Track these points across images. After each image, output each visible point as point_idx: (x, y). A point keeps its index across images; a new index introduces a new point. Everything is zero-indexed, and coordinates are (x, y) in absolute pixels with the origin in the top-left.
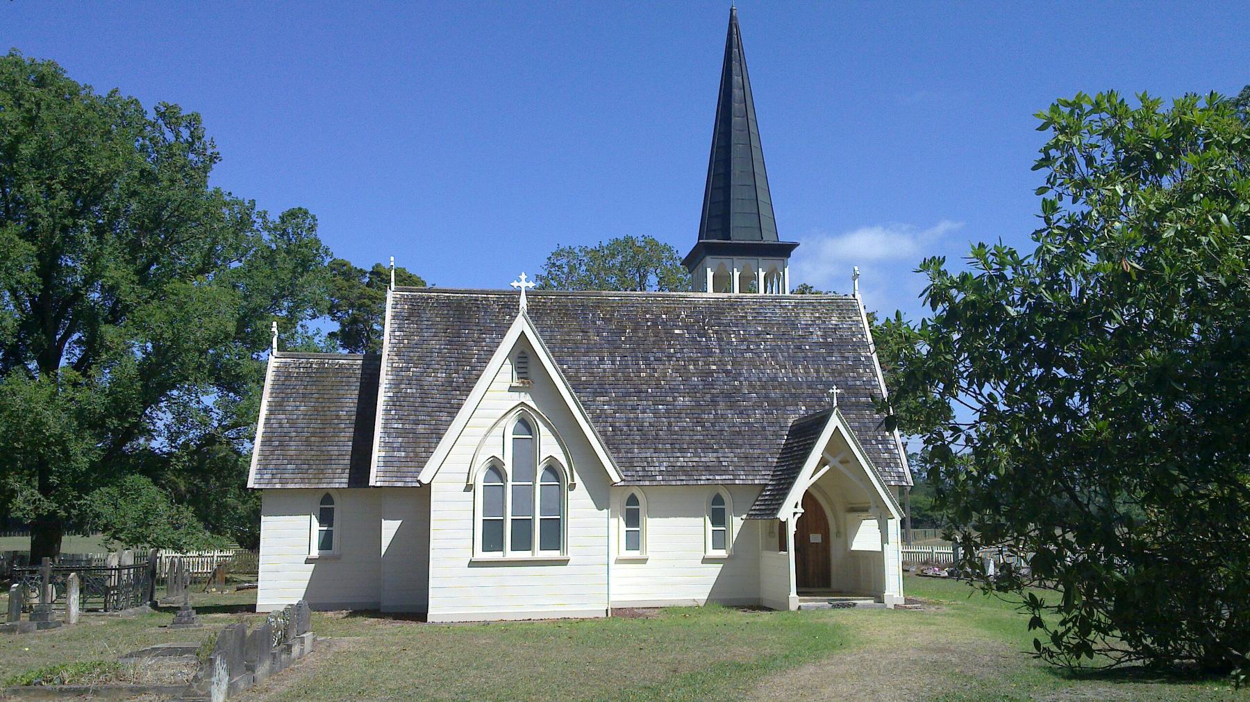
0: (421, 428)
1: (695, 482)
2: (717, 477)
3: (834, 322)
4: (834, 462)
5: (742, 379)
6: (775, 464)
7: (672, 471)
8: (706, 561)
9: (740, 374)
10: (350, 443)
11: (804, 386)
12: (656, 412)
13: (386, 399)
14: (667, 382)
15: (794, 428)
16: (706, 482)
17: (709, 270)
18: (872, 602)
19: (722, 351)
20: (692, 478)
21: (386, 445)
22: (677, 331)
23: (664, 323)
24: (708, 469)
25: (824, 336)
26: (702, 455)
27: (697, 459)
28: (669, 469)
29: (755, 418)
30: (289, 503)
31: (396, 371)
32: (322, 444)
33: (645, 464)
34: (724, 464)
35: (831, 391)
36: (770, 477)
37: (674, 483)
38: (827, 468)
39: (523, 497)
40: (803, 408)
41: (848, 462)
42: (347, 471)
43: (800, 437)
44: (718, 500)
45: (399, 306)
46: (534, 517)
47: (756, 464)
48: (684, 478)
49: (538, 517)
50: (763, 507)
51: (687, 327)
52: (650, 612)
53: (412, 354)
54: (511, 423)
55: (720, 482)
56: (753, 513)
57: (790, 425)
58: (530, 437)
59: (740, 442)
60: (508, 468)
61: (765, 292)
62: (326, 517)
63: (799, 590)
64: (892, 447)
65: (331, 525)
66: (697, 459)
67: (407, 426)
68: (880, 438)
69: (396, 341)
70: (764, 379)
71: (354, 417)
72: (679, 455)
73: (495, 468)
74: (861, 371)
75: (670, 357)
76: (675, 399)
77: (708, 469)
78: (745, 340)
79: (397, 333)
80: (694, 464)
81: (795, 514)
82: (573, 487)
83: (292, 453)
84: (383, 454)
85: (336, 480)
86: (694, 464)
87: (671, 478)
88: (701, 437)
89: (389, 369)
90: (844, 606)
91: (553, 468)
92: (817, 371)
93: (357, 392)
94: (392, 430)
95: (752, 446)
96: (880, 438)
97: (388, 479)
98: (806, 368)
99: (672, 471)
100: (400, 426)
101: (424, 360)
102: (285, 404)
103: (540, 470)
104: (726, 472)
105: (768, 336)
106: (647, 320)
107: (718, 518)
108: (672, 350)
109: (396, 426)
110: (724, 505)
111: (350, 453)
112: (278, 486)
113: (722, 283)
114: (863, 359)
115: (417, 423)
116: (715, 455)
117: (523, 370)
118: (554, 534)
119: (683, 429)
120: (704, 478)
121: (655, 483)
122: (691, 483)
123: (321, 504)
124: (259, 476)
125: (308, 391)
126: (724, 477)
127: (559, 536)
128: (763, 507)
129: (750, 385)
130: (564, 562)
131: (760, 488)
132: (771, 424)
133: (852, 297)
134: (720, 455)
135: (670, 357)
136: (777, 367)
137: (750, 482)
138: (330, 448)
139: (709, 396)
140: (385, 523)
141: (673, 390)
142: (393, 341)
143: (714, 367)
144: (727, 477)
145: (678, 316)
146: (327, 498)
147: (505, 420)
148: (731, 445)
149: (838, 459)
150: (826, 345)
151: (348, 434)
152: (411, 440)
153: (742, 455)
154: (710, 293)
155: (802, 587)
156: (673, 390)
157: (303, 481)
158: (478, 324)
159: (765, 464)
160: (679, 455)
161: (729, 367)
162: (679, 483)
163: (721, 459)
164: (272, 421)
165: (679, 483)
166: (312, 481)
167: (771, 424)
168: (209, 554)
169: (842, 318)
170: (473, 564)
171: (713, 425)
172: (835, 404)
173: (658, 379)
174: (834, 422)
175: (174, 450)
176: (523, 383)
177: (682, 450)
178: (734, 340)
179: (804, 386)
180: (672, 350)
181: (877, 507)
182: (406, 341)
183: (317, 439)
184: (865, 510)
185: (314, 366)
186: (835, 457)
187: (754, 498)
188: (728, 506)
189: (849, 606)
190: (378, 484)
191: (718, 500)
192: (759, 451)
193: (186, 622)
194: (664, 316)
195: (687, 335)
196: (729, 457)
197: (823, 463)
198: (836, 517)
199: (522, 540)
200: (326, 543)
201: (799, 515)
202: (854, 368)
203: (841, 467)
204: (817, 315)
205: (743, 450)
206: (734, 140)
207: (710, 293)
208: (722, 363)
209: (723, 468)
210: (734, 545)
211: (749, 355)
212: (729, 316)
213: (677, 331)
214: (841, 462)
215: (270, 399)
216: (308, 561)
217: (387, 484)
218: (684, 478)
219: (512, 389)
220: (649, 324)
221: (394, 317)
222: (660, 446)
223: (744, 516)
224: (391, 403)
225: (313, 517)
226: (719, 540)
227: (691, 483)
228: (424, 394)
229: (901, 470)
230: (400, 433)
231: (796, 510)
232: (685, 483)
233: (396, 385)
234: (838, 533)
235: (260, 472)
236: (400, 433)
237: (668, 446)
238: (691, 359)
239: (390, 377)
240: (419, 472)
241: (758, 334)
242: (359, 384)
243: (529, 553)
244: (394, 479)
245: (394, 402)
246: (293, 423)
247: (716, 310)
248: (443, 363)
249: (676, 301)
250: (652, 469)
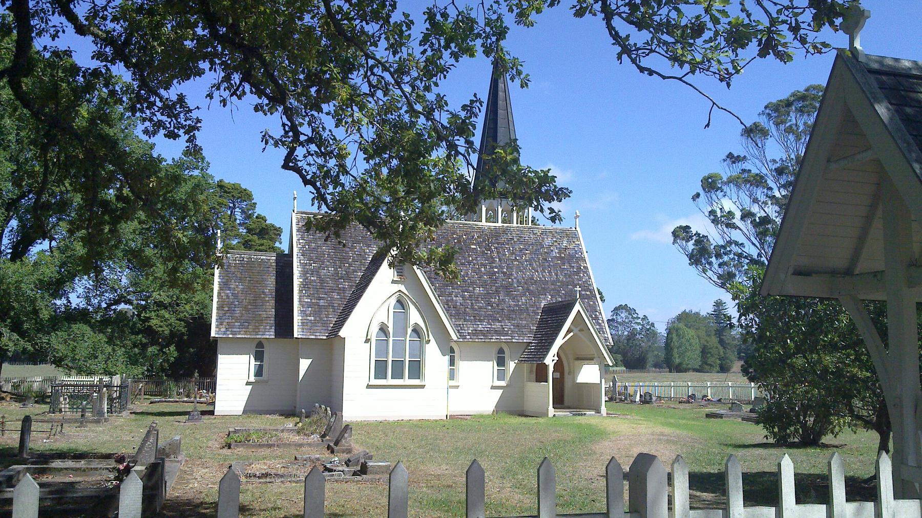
0: (322, 302)
1: (489, 340)
2: (502, 338)
3: (565, 245)
4: (576, 330)
5: (513, 278)
6: (535, 331)
7: (476, 333)
8: (493, 388)
9: (512, 275)
10: (273, 310)
11: (550, 283)
12: (463, 297)
13: (299, 283)
14: (469, 278)
15: (546, 309)
16: (496, 340)
17: (483, 206)
18: (594, 413)
19: (500, 260)
20: (487, 337)
21: (303, 313)
22: (473, 247)
23: (465, 241)
24: (497, 332)
25: (560, 253)
26: (492, 324)
27: (489, 326)
28: (474, 332)
29: (522, 302)
30: (237, 347)
31: (303, 265)
32: (256, 310)
33: (459, 328)
34: (505, 329)
35: (576, 289)
36: (532, 338)
37: (477, 340)
38: (572, 334)
39: (399, 347)
40: (550, 297)
41: (583, 330)
42: (273, 327)
43: (552, 315)
44: (501, 351)
45: (300, 223)
46: (405, 359)
47: (524, 330)
48: (482, 337)
49: (407, 359)
50: (531, 356)
51: (478, 244)
52: (36, 434)
53: (312, 255)
54: (393, 301)
55: (504, 341)
56: (523, 359)
57: (542, 307)
58: (404, 311)
59: (514, 316)
60: (391, 329)
61: (517, 224)
62: (259, 356)
63: (555, 406)
64: (600, 322)
65: (262, 361)
66: (489, 326)
67: (313, 301)
68: (594, 316)
69: (301, 246)
70: (526, 279)
71: (274, 294)
72: (479, 323)
73: (383, 329)
74: (582, 275)
75: (469, 262)
76: (474, 289)
77: (497, 332)
78: (513, 253)
79: (301, 241)
80: (488, 329)
81: (553, 360)
82: (428, 342)
83: (237, 315)
84: (300, 318)
85: (267, 333)
86: (488, 329)
87: (475, 337)
88: (491, 313)
89: (299, 264)
90: (579, 415)
91: (416, 330)
92: (556, 275)
93: (274, 277)
94: (304, 303)
95: (521, 319)
96: (594, 316)
97: (305, 334)
98: (550, 272)
99: (476, 333)
100: (309, 300)
101: (319, 259)
102: (229, 283)
103: (409, 331)
104: (507, 334)
105: (527, 252)
106: (454, 239)
107: (501, 362)
108: (471, 258)
109: (306, 300)
110: (263, 348)
111: (274, 316)
112: (231, 336)
113: (492, 218)
114: (582, 268)
115: (320, 298)
116: (500, 324)
117: (401, 271)
118: (417, 369)
119: (480, 308)
120: (494, 338)
121: (466, 340)
122: (487, 340)
123: (498, 354)
124: (217, 329)
125: (243, 276)
126: (506, 337)
127: (420, 373)
128: (531, 356)
129: (518, 281)
130: (423, 387)
131: (526, 345)
132: (532, 306)
133: (574, 229)
134: (503, 324)
135: (469, 262)
136: (533, 271)
137: (521, 341)
138: (260, 313)
139: (494, 288)
140: (302, 361)
141: (473, 283)
142: (299, 246)
143: (496, 270)
144: (508, 338)
145: (473, 237)
146: (260, 344)
147: (389, 300)
148: (509, 319)
149: (579, 328)
150: (561, 258)
151: (271, 304)
152: (317, 310)
153: (515, 324)
154: (515, 224)
155: (556, 404)
156: (473, 283)
157: (246, 333)
158: (351, 237)
159: (529, 330)
160: (479, 323)
161: (505, 270)
162: (480, 340)
163: (504, 327)
164: (222, 294)
165: (480, 340)
166: (252, 333)
167: (532, 306)
168: (91, 379)
169: (569, 242)
170: (369, 387)
171: (498, 305)
172: (578, 297)
173: (463, 276)
174: (577, 307)
175: (89, 307)
176: (401, 278)
177: (480, 321)
178: (507, 253)
179: (550, 283)
180: (471, 258)
181: (599, 357)
182: (307, 247)
183: (252, 307)
184: (592, 359)
185: (245, 259)
186: (576, 328)
187: (523, 351)
188: (507, 355)
189: (582, 415)
190: (300, 337)
191: (501, 351)
192: (525, 322)
193: (196, 419)
194: (464, 237)
195: (479, 249)
196: (508, 325)
197: (569, 331)
198: (569, 364)
199: (398, 374)
200: (259, 372)
201: (555, 361)
202: (577, 273)
203: (580, 334)
204: (555, 239)
205: (516, 322)
206: (499, 124)
207: (515, 224)
208: (501, 267)
209: (505, 332)
210: (510, 379)
211: (516, 263)
212: (503, 239)
213: (473, 247)
214: (579, 331)
215: (219, 280)
216: (248, 384)
217: (304, 337)
218: (482, 337)
219: (393, 282)
220: (456, 241)
221: (298, 231)
222: (467, 318)
223: (516, 361)
224: (302, 286)
225: (251, 356)
226: (501, 376)
227: (487, 340)
228: (322, 281)
229: (606, 336)
230: (310, 305)
231: (554, 358)
232: (483, 340)
233: (304, 273)
234: (569, 373)
235: (217, 327)
236: (310, 305)
237: (472, 318)
238: (482, 265)
239: (300, 269)
240: (339, 331)
241: (521, 250)
242: (275, 272)
243: (402, 380)
244: (309, 334)
245: (305, 286)
246: (235, 296)
247: (496, 233)
248: (331, 261)
249: (471, 227)
250: (463, 331)
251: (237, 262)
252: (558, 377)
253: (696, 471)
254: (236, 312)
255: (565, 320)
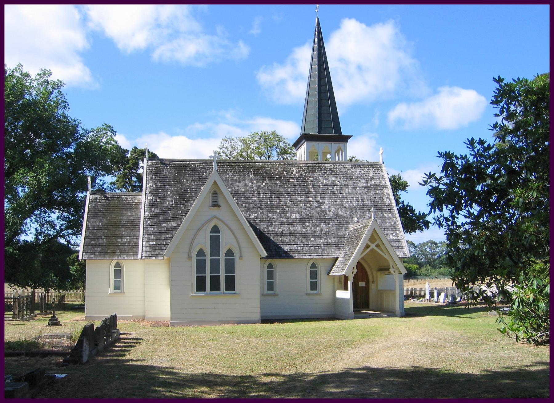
3: (371, 176)
20: (300, 255)
63: (355, 310)
68: (394, 234)
80: (301, 248)
144: (318, 254)
201: (355, 273)
204: (363, 172)
231: (353, 270)
234: (373, 282)
251: (103, 201)
252: (364, 285)
253: (218, 326)
254: (162, 218)
255: (214, 257)
